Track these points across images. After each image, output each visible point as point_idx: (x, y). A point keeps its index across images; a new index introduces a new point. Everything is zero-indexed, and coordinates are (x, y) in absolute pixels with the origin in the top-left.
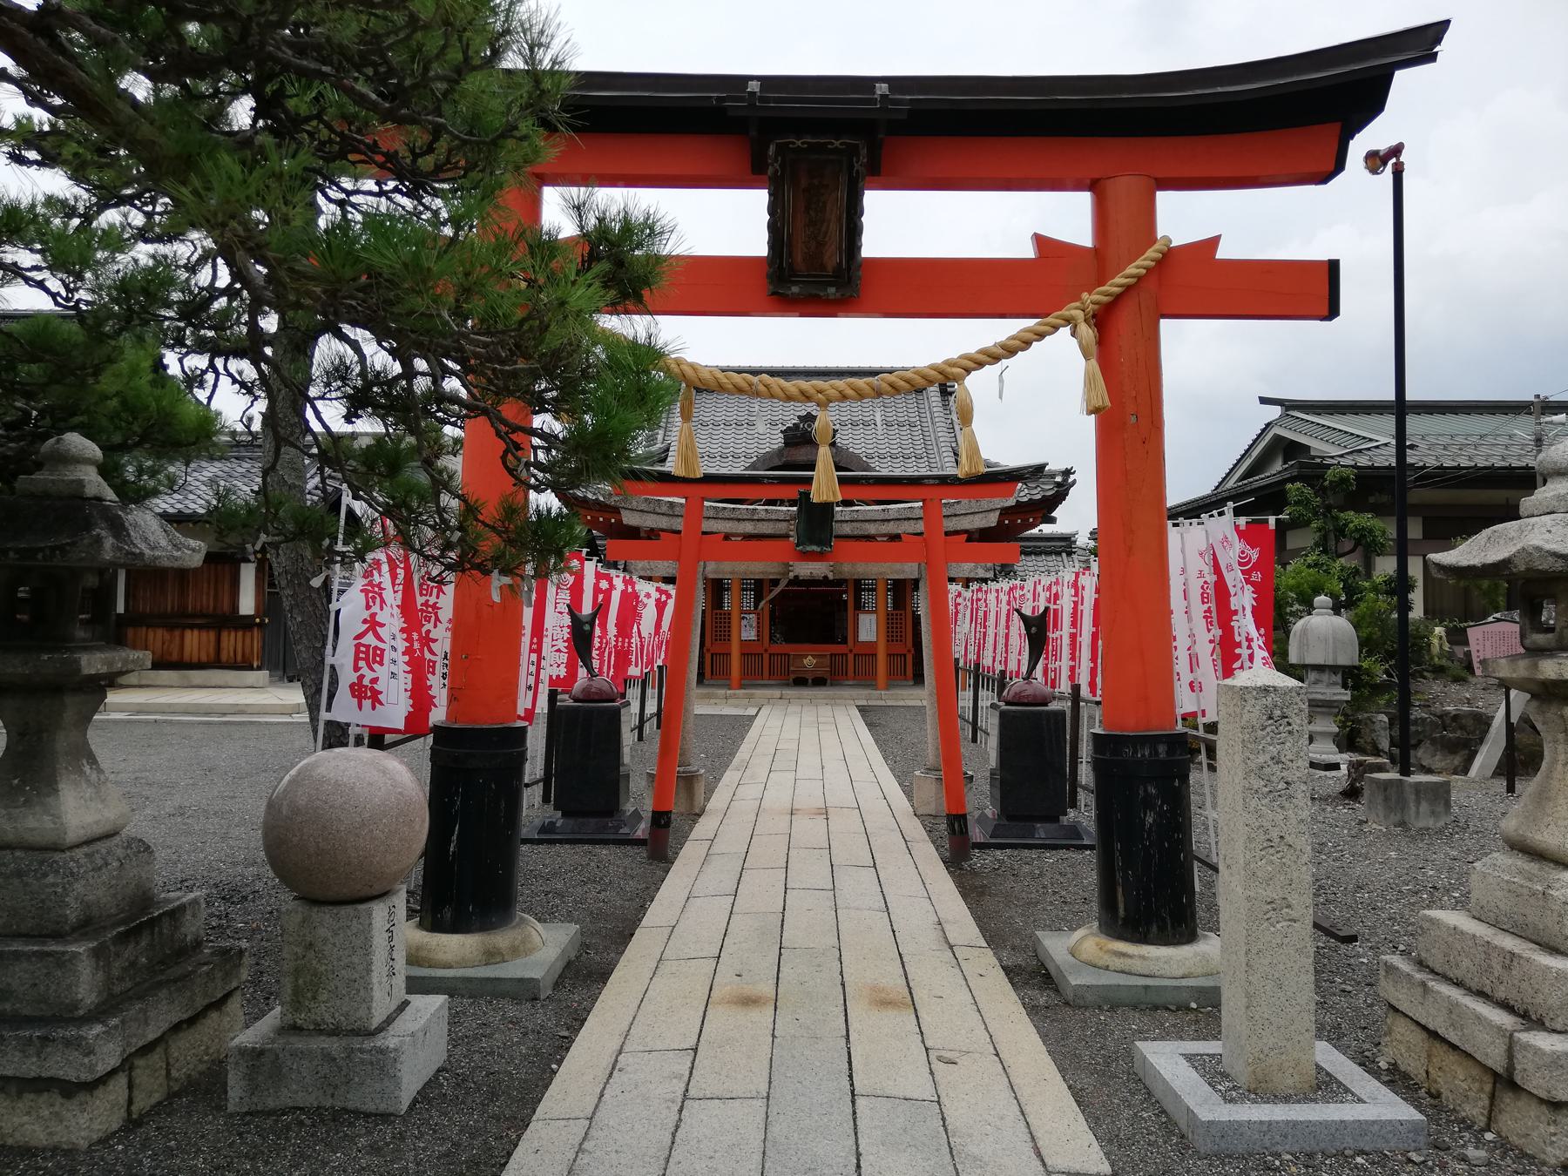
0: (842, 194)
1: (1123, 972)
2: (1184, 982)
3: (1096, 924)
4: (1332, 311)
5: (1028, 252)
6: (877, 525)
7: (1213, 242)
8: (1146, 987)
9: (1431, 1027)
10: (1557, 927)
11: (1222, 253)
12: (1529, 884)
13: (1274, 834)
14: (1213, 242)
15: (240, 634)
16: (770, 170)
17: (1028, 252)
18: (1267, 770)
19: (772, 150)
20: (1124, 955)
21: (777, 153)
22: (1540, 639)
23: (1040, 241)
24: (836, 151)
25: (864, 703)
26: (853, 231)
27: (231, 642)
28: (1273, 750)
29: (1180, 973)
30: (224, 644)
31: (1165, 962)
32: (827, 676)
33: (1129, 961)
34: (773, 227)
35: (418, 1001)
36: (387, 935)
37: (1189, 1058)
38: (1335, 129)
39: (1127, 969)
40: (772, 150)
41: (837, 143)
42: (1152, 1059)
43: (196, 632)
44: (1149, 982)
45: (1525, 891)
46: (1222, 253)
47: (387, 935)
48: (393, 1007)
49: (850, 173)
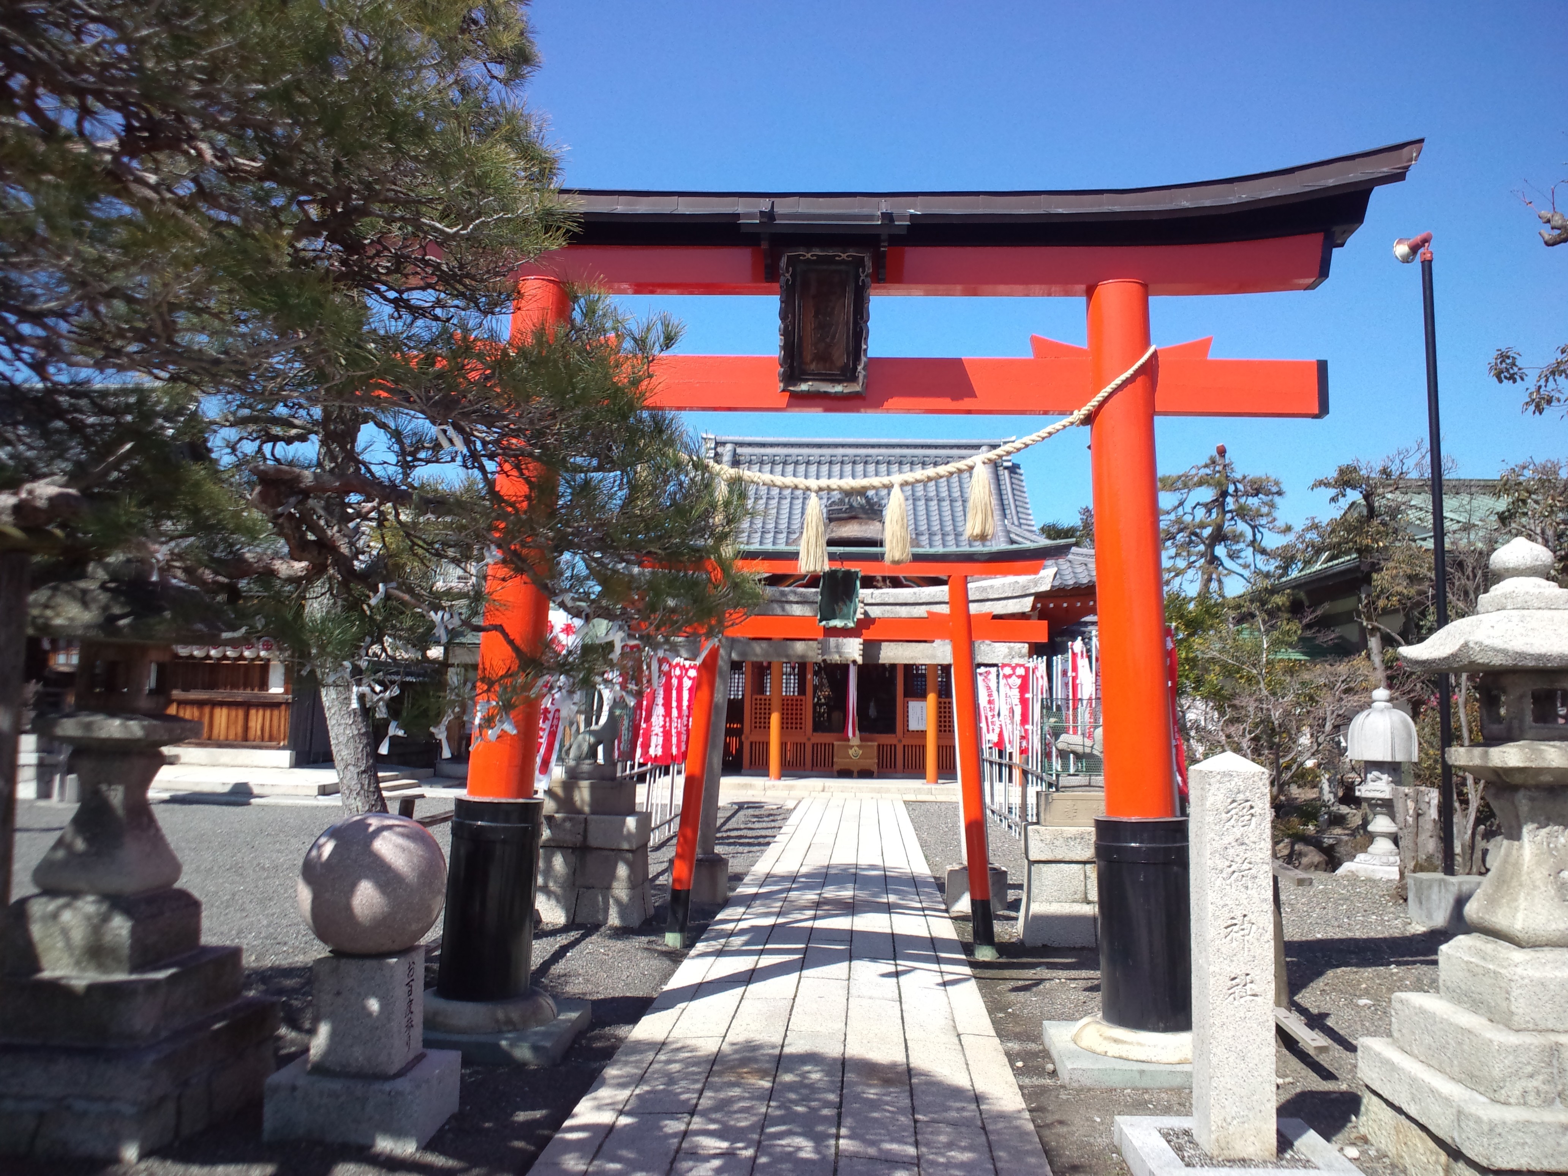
0: (849, 301)
1: (1120, 1058)
2: (1179, 1068)
3: (1100, 1015)
4: (1323, 409)
5: (1027, 353)
6: (908, 608)
7: (1204, 345)
8: (1142, 1072)
9: (1396, 1103)
10: (1504, 1004)
11: (1214, 355)
12: (1482, 963)
13: (1238, 914)
14: (1204, 345)
15: (268, 713)
16: (782, 279)
17: (1027, 353)
18: (1231, 851)
19: (784, 260)
20: (1116, 1041)
21: (788, 265)
22: (1495, 728)
23: (1036, 342)
24: (843, 262)
25: (912, 797)
26: (859, 334)
27: (257, 719)
28: (1238, 832)
29: (1175, 1059)
30: (252, 724)
31: (1156, 1049)
32: (875, 768)
33: (1126, 1047)
34: (787, 333)
35: (434, 1055)
36: (407, 989)
37: (1167, 1136)
38: (1316, 240)
39: (1124, 1055)
40: (784, 260)
41: (844, 256)
42: (1126, 1130)
43: (225, 711)
44: (1144, 1067)
45: (1481, 971)
46: (1214, 355)
47: (407, 989)
48: (411, 1056)
49: (857, 282)
